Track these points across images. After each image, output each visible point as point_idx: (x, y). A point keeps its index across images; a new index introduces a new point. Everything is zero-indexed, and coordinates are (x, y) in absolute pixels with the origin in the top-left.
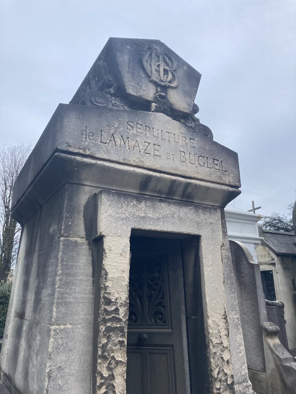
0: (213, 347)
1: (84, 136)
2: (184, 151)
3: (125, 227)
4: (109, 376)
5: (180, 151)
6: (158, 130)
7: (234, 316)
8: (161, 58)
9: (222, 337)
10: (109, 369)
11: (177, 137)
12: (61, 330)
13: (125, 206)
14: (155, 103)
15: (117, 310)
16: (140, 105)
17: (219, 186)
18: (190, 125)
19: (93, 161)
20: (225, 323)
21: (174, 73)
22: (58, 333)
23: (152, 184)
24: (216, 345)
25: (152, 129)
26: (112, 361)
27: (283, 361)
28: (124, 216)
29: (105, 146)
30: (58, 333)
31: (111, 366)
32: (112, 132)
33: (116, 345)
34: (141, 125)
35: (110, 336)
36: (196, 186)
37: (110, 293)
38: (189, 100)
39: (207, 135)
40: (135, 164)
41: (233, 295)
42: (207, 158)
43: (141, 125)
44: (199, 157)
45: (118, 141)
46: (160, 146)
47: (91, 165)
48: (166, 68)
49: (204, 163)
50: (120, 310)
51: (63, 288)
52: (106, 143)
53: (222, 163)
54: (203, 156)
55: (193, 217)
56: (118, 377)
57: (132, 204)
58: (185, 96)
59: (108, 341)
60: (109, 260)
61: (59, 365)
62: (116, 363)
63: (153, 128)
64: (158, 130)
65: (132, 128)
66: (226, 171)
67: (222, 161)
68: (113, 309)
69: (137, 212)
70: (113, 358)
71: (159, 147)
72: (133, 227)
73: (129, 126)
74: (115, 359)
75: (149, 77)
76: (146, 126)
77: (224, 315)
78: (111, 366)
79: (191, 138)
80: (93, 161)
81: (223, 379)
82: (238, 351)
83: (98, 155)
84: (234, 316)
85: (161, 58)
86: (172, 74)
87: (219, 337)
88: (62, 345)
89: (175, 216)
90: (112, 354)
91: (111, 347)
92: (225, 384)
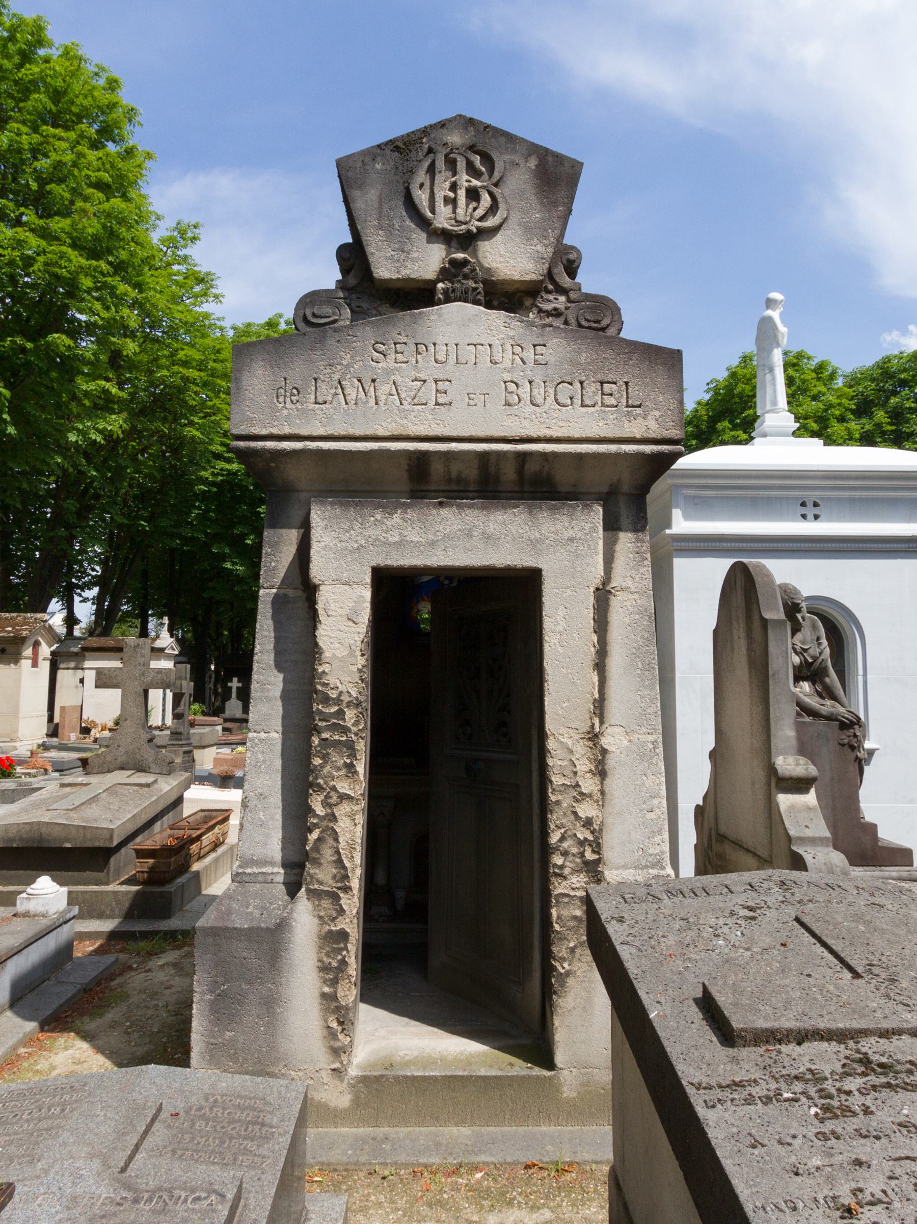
0: (554, 790)
1: (281, 399)
2: (515, 380)
3: (357, 567)
4: (327, 815)
5: (505, 382)
6: (446, 345)
7: (643, 737)
8: (461, 164)
9: (579, 774)
10: (326, 804)
11: (497, 349)
12: (261, 740)
13: (357, 526)
14: (442, 281)
15: (340, 714)
16: (415, 296)
17: (613, 448)
18: (548, 307)
19: (298, 445)
20: (591, 748)
21: (495, 190)
22: (257, 745)
23: (437, 469)
24: (562, 789)
25: (431, 348)
26: (333, 794)
27: (793, 842)
28: (356, 546)
29: (322, 410)
30: (257, 745)
31: (329, 801)
32: (337, 377)
33: (339, 769)
34: (405, 343)
35: (328, 754)
36: (544, 455)
37: (328, 684)
38: (539, 248)
39: (600, 318)
40: (388, 434)
41: (647, 692)
42: (581, 383)
43: (405, 343)
44: (558, 384)
45: (352, 394)
46: (450, 381)
47: (294, 452)
48: (475, 183)
49: (571, 398)
50: (347, 713)
51: (263, 675)
52: (325, 403)
53: (627, 389)
54: (568, 379)
55: (521, 531)
56: (344, 818)
57: (372, 519)
58: (529, 239)
59: (326, 762)
60: (325, 627)
61: (260, 791)
62: (338, 797)
63: (434, 344)
64: (446, 345)
65: (385, 356)
66: (639, 406)
67: (627, 383)
68: (332, 710)
69: (384, 535)
70: (334, 788)
71: (448, 383)
72: (374, 564)
73: (375, 354)
74: (337, 791)
75: (424, 223)
76: (416, 344)
77: (589, 733)
78: (329, 801)
79: (536, 343)
80: (298, 445)
81: (575, 850)
82: (644, 806)
83: (304, 432)
84: (643, 737)
85: (461, 164)
86: (491, 194)
87: (571, 775)
88: (264, 762)
89: (475, 533)
90: (332, 783)
91: (329, 772)
92: (578, 860)
